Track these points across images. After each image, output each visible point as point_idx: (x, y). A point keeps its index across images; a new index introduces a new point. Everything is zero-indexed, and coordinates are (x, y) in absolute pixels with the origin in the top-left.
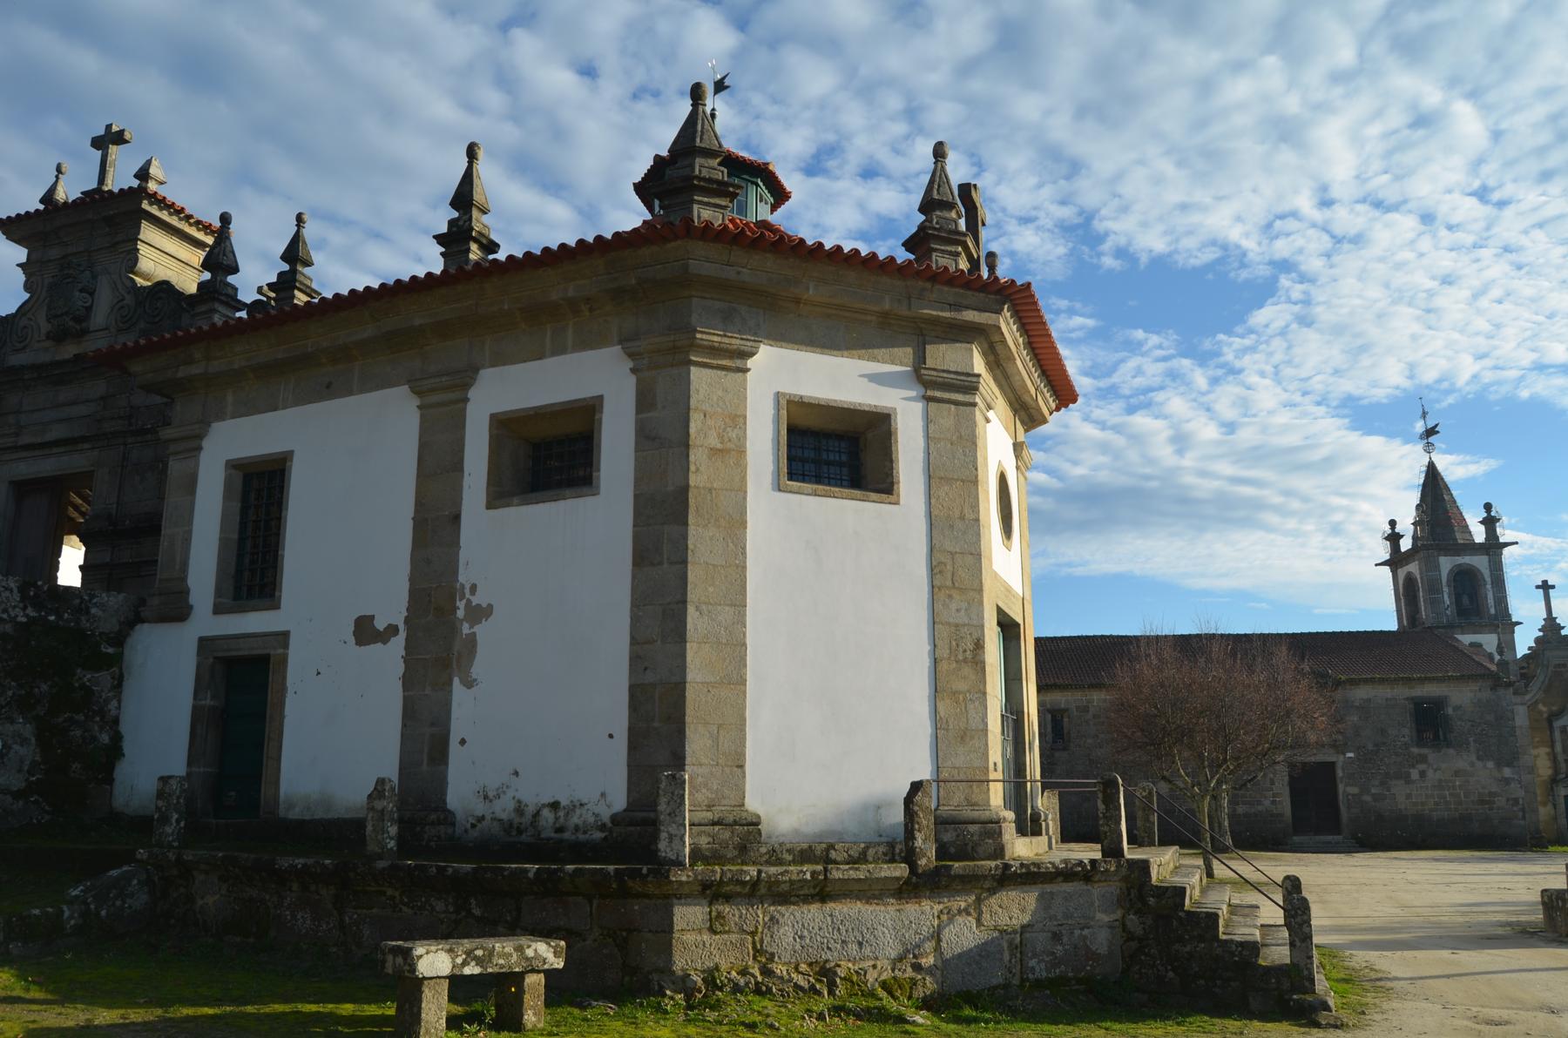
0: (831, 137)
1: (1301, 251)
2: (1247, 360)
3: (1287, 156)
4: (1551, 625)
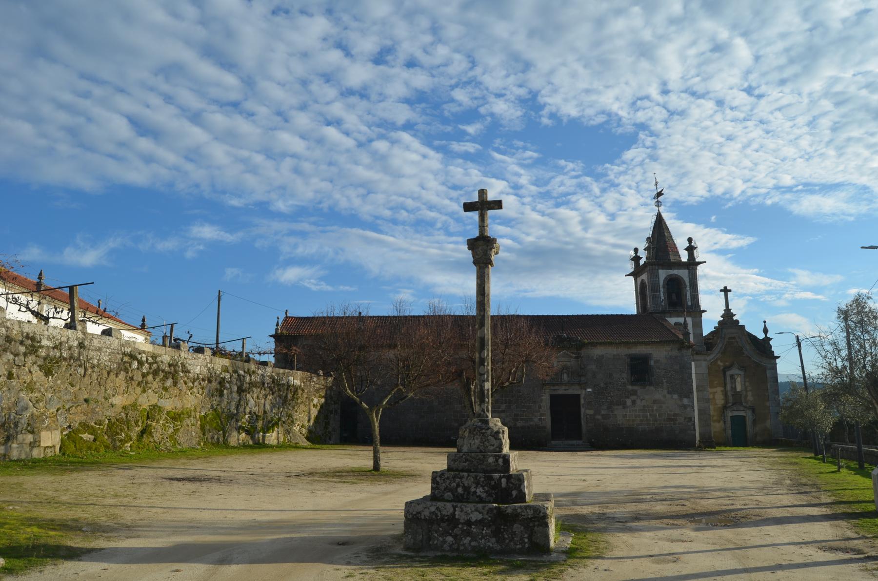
0: (388, 43)
1: (651, 118)
3: (644, 64)
4: (728, 314)
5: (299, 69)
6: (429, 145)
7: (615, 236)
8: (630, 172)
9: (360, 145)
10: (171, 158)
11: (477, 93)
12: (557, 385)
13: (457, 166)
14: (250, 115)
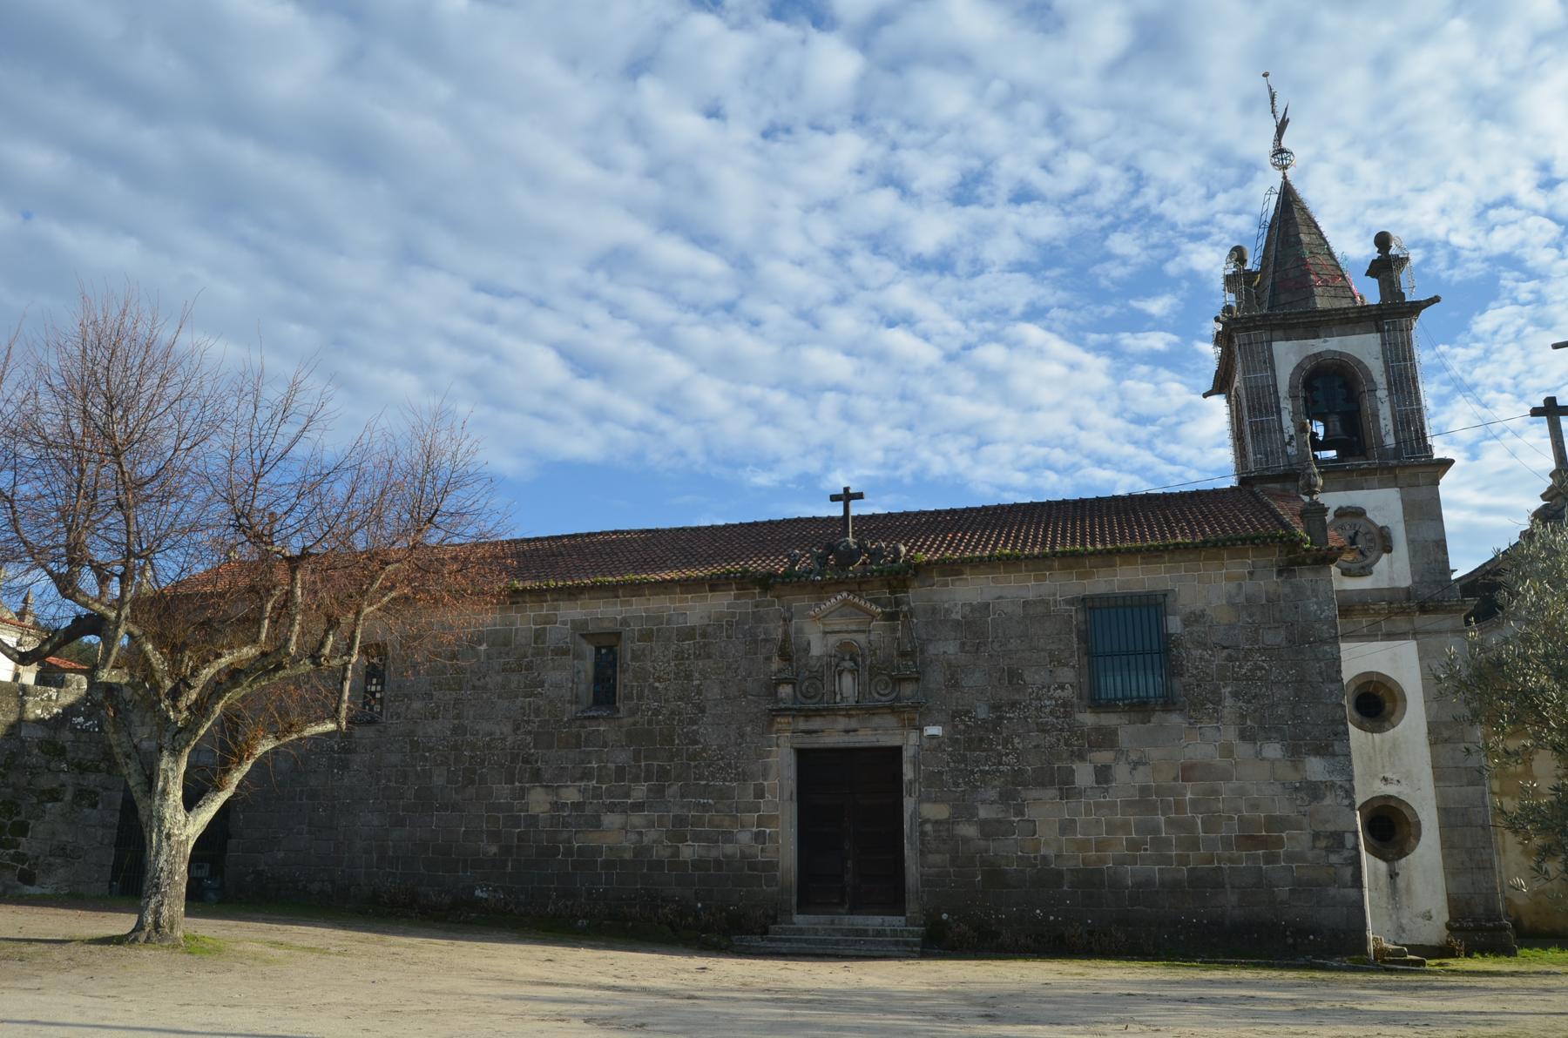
0: (975, 164)
1: (1523, 244)
2: (1478, 373)
3: (1494, 134)
5: (825, 231)
6: (1080, 342)
7: (1483, 489)
8: (1496, 356)
9: (951, 358)
10: (634, 410)
11: (1156, 237)
12: (817, 713)
13: (1141, 379)
14: (755, 323)
